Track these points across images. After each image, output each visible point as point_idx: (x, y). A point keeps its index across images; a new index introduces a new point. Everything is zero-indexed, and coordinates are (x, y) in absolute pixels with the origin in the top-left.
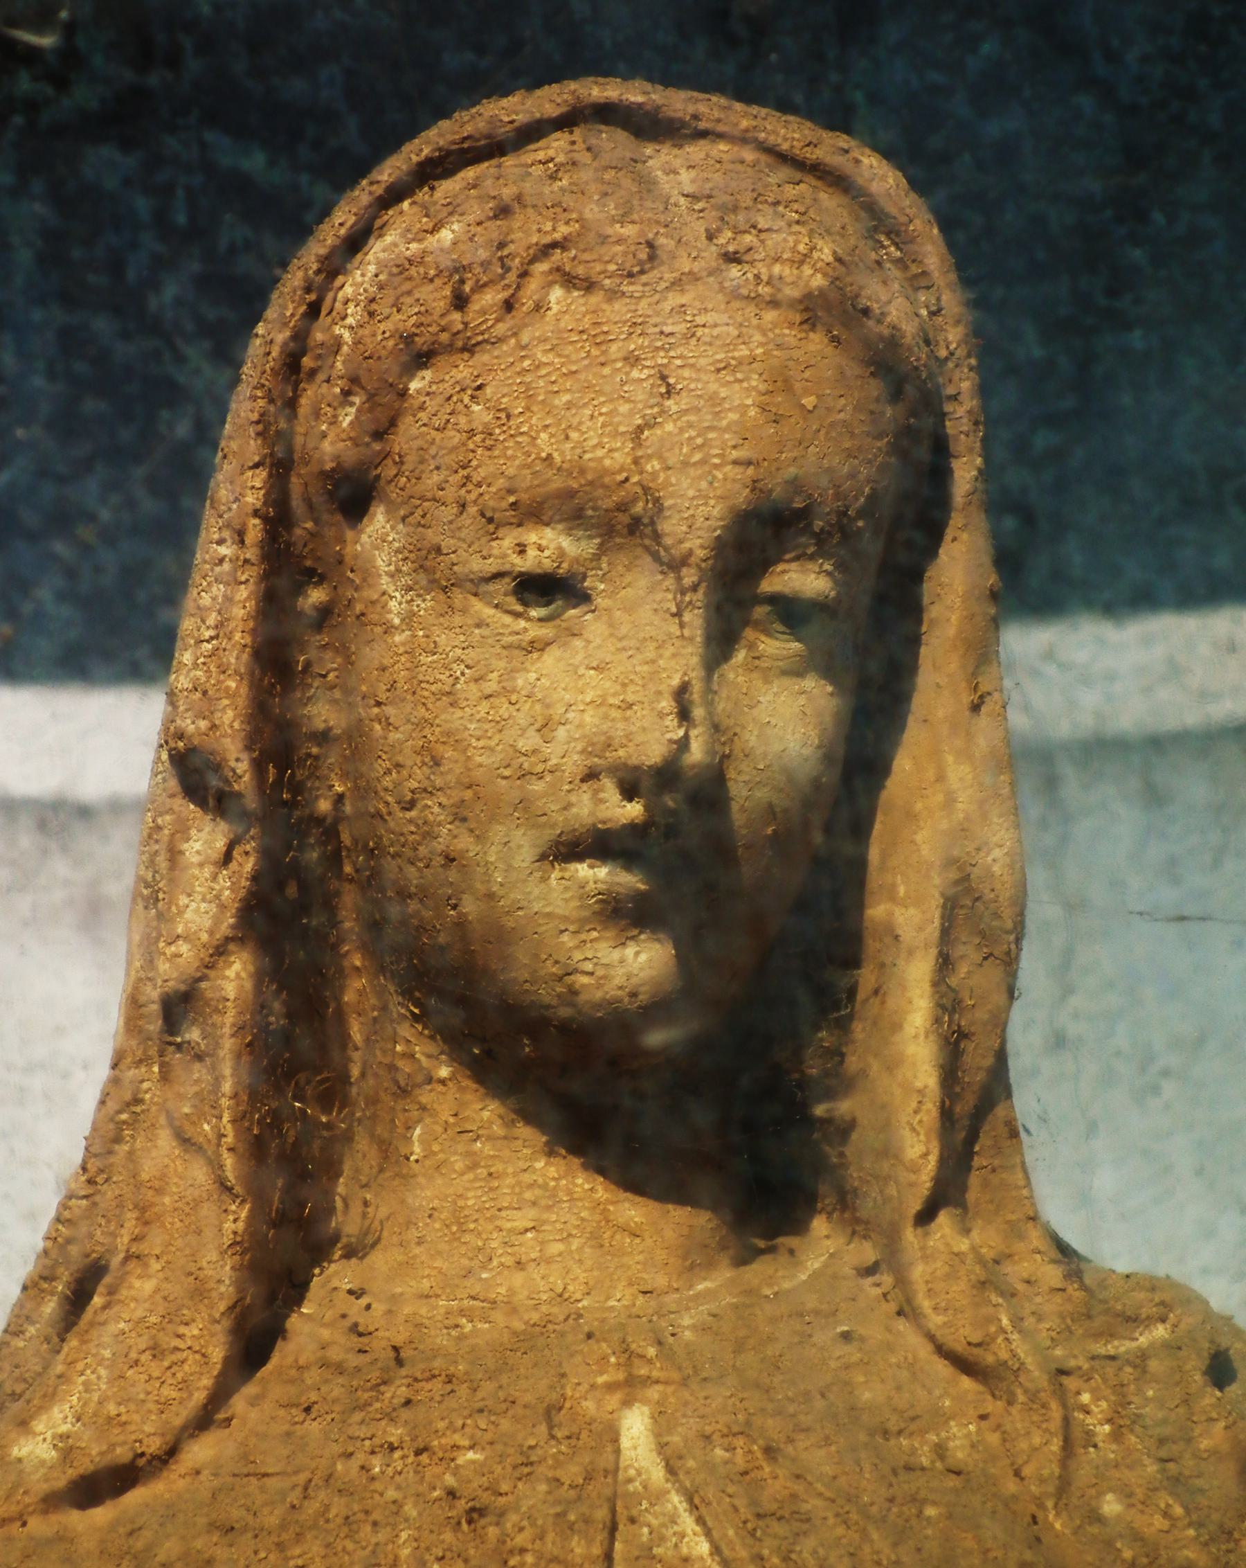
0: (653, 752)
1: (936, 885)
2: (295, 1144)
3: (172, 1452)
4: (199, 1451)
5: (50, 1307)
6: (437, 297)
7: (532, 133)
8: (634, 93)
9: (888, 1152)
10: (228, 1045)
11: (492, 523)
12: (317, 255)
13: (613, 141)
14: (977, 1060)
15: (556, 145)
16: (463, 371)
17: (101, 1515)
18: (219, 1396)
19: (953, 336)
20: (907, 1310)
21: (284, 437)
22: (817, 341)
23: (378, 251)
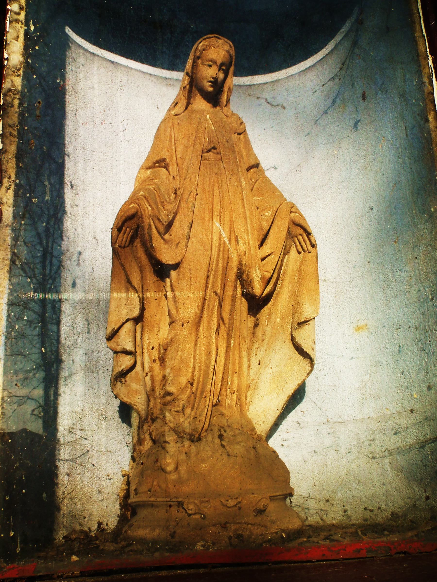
0: (215, 76)
1: (228, 87)
2: (87, 60)
3: (181, 114)
4: (183, 114)
5: (174, 104)
6: (205, 47)
7: (212, 37)
8: (218, 36)
9: (223, 102)
10: (187, 90)
11: (207, 61)
12: (184, 501)
13: (217, 39)
14: (228, 98)
15: (213, 38)
16: (206, 51)
17: (177, 117)
18: (184, 111)
19: (234, 54)
20: (223, 112)
21: (208, 356)
22: (227, 53)
23: (202, 43)
